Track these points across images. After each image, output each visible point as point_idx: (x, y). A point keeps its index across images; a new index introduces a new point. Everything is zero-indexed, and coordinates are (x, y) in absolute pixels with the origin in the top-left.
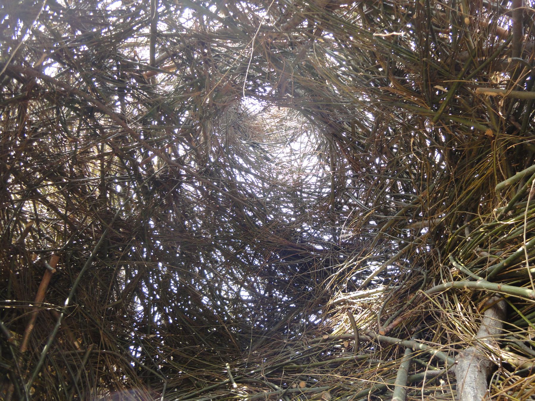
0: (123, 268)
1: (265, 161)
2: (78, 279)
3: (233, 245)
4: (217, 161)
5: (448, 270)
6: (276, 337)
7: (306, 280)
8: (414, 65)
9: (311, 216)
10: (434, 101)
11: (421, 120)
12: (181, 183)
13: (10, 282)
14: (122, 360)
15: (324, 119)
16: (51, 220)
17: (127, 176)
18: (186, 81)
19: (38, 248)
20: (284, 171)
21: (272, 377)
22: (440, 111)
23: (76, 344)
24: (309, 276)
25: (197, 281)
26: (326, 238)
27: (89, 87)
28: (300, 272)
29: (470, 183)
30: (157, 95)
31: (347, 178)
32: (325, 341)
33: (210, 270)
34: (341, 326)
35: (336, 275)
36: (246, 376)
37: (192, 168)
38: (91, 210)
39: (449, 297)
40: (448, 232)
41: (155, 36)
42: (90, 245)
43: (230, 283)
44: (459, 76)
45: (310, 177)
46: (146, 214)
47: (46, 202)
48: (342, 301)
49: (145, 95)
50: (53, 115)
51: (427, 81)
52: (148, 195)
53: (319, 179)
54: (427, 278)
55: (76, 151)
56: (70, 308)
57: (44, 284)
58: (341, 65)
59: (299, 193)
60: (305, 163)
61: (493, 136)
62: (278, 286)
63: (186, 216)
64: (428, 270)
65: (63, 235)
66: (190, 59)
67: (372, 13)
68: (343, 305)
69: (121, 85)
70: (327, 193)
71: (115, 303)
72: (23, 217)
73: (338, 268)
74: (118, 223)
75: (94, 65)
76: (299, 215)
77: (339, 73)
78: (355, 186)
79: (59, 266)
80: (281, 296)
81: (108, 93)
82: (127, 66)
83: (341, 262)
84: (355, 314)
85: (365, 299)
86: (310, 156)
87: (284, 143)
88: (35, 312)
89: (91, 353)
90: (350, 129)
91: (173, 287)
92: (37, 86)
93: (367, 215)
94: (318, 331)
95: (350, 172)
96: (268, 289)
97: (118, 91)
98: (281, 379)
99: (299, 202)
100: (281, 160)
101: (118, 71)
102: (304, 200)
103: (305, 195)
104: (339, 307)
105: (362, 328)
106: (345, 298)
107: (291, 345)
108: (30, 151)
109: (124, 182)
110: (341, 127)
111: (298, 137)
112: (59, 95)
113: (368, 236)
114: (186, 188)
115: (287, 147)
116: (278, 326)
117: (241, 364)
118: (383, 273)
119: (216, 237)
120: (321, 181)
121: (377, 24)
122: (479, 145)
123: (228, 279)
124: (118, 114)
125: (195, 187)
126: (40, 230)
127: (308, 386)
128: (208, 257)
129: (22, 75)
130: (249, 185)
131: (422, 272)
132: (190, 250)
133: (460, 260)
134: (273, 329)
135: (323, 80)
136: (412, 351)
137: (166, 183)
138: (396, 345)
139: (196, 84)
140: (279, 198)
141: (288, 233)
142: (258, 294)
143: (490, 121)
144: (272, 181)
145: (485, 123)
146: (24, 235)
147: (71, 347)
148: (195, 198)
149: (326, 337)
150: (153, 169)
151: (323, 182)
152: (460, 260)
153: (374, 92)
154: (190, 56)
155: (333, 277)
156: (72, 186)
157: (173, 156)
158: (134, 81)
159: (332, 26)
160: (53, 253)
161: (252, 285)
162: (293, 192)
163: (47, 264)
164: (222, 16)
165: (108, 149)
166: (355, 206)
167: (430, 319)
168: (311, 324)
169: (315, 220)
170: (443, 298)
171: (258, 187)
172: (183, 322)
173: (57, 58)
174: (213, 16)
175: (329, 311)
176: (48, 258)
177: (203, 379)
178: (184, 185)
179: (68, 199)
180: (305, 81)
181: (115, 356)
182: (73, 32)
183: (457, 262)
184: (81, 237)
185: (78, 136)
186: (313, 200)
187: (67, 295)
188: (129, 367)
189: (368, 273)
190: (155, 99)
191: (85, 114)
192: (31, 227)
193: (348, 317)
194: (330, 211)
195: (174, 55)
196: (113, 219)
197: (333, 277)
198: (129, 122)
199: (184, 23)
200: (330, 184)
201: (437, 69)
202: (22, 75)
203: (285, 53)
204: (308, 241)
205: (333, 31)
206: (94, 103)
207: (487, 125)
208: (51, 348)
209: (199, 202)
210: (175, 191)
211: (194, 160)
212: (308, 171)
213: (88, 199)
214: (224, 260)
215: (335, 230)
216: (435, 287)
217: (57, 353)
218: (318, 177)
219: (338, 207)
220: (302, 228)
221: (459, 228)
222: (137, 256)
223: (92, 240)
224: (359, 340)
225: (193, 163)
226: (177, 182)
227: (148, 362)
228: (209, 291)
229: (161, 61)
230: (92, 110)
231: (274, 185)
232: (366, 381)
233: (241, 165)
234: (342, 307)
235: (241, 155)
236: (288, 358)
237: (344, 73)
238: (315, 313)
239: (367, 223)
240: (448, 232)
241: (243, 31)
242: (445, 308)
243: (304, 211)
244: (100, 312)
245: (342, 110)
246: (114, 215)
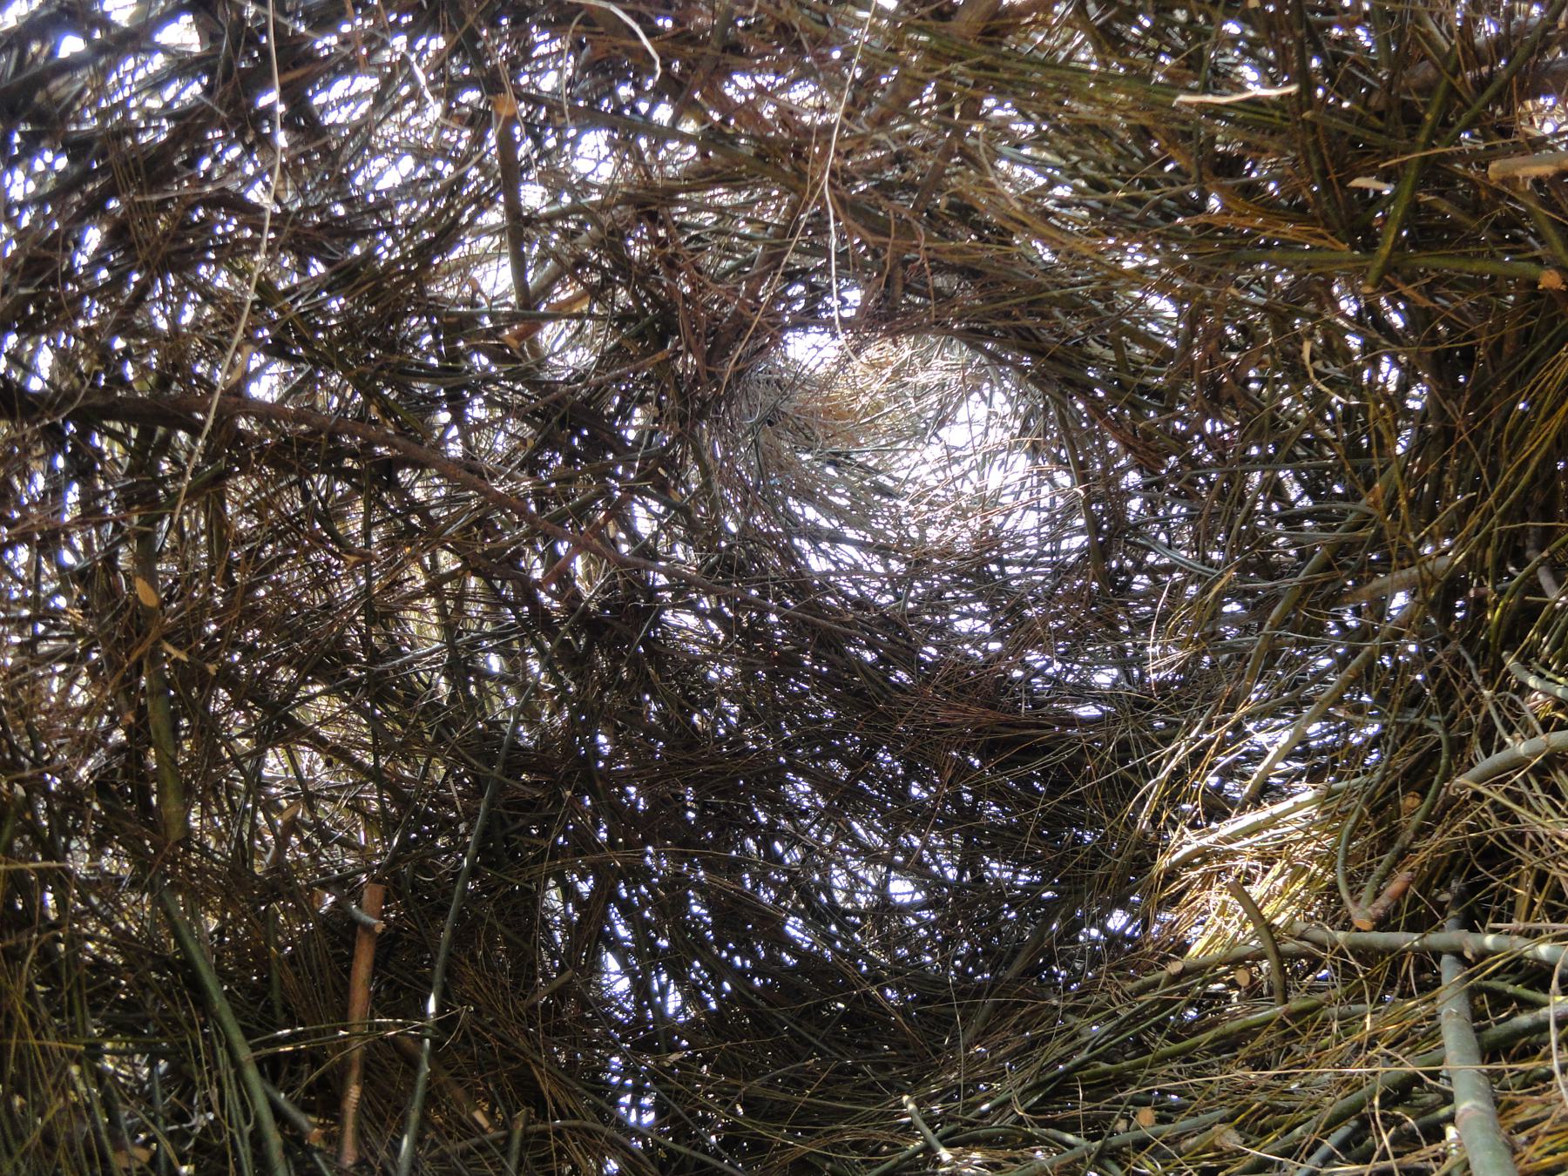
2: (445, 936)
4: (745, 527)
5: (1512, 702)
6: (1022, 994)
7: (1072, 810)
8: (1272, 134)
9: (1044, 625)
10: (1356, 222)
11: (1320, 284)
12: (661, 611)
13: (275, 977)
14: (610, 1140)
15: (1027, 341)
16: (340, 788)
19: (325, 873)
20: (941, 515)
21: (1044, 1112)
22: (1384, 251)
23: (479, 1116)
24: (1078, 800)
25: (761, 878)
26: (1104, 678)
27: (373, 408)
28: (1051, 794)
30: (550, 386)
32: (1175, 979)
33: (792, 840)
34: (1210, 927)
38: (439, 739)
39: (1540, 781)
41: (520, 226)
42: (453, 835)
43: (853, 864)
44: (1422, 138)
45: (1016, 516)
46: (588, 716)
47: (319, 743)
48: (1195, 853)
50: (292, 502)
52: (577, 663)
53: (1044, 515)
54: (1450, 740)
55: (369, 585)
56: (445, 1024)
58: (1052, 183)
59: (994, 568)
60: (994, 478)
62: (993, 846)
63: (693, 701)
65: (382, 824)
66: (623, 264)
67: (1117, 18)
69: (452, 381)
71: (556, 984)
72: (268, 795)
73: (1159, 762)
74: (517, 758)
75: (372, 342)
76: (1010, 631)
77: (1049, 204)
78: (1155, 513)
80: (1007, 875)
81: (422, 410)
82: (456, 325)
83: (1167, 741)
87: (918, 435)
88: (357, 1049)
89: (526, 1135)
90: (1110, 355)
92: (241, 435)
93: (1216, 589)
94: (1145, 955)
95: (1133, 478)
96: (969, 862)
98: (1079, 1112)
99: (1000, 592)
101: (436, 344)
102: (1014, 583)
104: (1192, 874)
106: (1204, 842)
107: (1073, 1010)
108: (252, 615)
109: (509, 644)
111: (957, 407)
112: (299, 447)
113: (1228, 648)
114: (674, 621)
116: (1019, 965)
118: (1300, 750)
120: (1050, 521)
121: (1137, 45)
122: (1521, 322)
123: (844, 853)
124: (456, 461)
125: (701, 614)
127: (1161, 1120)
128: (779, 804)
131: (1427, 723)
132: (723, 791)
133: (1548, 667)
134: (1009, 975)
135: (1003, 236)
136: (1467, 963)
139: (648, 331)
140: (940, 593)
141: (982, 687)
142: (941, 881)
143: (1542, 243)
144: (912, 549)
146: (282, 843)
147: (471, 1129)
149: (1175, 967)
151: (1058, 524)
152: (1548, 667)
153: (1167, 238)
154: (622, 258)
158: (485, 361)
159: (1009, 82)
160: (364, 878)
161: (920, 861)
162: (978, 571)
165: (448, 561)
166: (1169, 569)
167: (1495, 856)
168: (1114, 940)
169: (1060, 634)
170: (1523, 789)
171: (873, 575)
172: (750, 1004)
173: (276, 350)
174: (662, 135)
176: (356, 893)
177: (846, 1151)
178: (668, 616)
180: (960, 251)
181: (590, 1133)
182: (303, 268)
183: (1541, 676)
185: (369, 543)
187: (430, 986)
188: (632, 1153)
189: (1256, 756)
191: (375, 479)
192: (294, 818)
194: (1098, 597)
198: (493, 476)
200: (1080, 522)
203: (886, 188)
205: (1015, 94)
207: (1538, 260)
208: (419, 1141)
209: (718, 653)
212: (1007, 500)
213: (424, 712)
215: (1123, 650)
216: (1484, 764)
217: (435, 1152)
218: (1039, 510)
220: (1025, 666)
221: (1520, 575)
225: (679, 548)
226: (648, 610)
227: (682, 1133)
228: (801, 898)
229: (545, 290)
230: (389, 467)
231: (919, 565)
233: (814, 523)
235: (807, 496)
236: (1079, 1049)
237: (1063, 203)
238: (1122, 903)
239: (1216, 615)
241: (757, 155)
243: (1021, 617)
245: (1073, 306)
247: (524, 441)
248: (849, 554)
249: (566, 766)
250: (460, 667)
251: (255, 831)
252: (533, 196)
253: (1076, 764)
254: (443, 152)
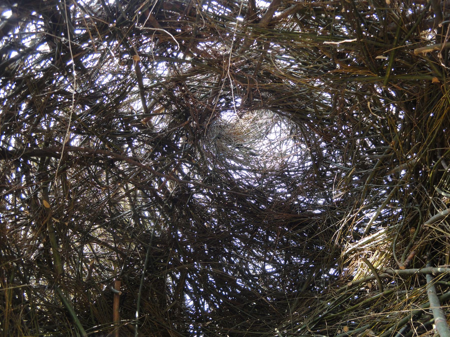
1: (251, 156)
4: (214, 169)
9: (302, 188)
10: (379, 68)
13: (91, 311)
15: (289, 109)
16: (106, 254)
17: (150, 203)
19: (103, 279)
24: (317, 237)
25: (228, 268)
28: (309, 237)
31: (322, 149)
32: (350, 287)
33: (236, 257)
34: (359, 271)
37: (198, 180)
38: (133, 237)
40: (426, 168)
41: (143, 90)
42: (139, 264)
44: (395, 44)
45: (291, 158)
46: (174, 227)
47: (98, 242)
48: (352, 250)
49: (147, 137)
50: (86, 174)
51: (368, 55)
52: (170, 211)
53: (299, 157)
54: (422, 212)
56: (141, 320)
57: (116, 305)
59: (286, 173)
61: (439, 82)
62: (294, 253)
63: (204, 219)
64: (419, 203)
65: (118, 263)
67: (305, 18)
69: (128, 136)
70: (310, 166)
71: (172, 305)
73: (339, 224)
74: (155, 241)
76: (293, 191)
77: (291, 70)
79: (122, 288)
82: (128, 120)
84: (368, 257)
85: (372, 243)
86: (286, 141)
87: (261, 137)
90: (313, 110)
91: (210, 279)
94: (341, 281)
95: (323, 144)
97: (127, 140)
99: (289, 180)
100: (264, 151)
102: (293, 177)
103: (292, 173)
104: (352, 256)
105: (378, 268)
106: (354, 247)
107: (322, 299)
112: (86, 158)
114: (197, 197)
115: (265, 139)
116: (305, 287)
117: (286, 326)
118: (379, 217)
120: (301, 158)
123: (251, 259)
124: (131, 158)
125: (204, 194)
126: (100, 265)
127: (350, 329)
130: (245, 179)
133: (447, 189)
136: (434, 277)
137: (181, 198)
138: (415, 274)
141: (286, 208)
143: (431, 70)
145: (429, 73)
146: (90, 271)
148: (206, 203)
149: (350, 284)
150: (168, 191)
151: (303, 159)
152: (447, 189)
155: (338, 232)
156: (114, 223)
157: (180, 176)
158: (137, 129)
159: (277, 38)
160: (114, 279)
162: (282, 174)
163: (113, 289)
164: (188, 58)
166: (336, 169)
170: (444, 225)
171: (252, 178)
173: (78, 132)
175: (344, 261)
176: (113, 284)
178: (195, 196)
179: (114, 234)
182: (83, 108)
184: (131, 260)
186: (300, 175)
187: (136, 309)
189: (367, 220)
190: (156, 137)
191: (108, 165)
192: (93, 264)
193: (362, 262)
194: (316, 179)
195: (160, 100)
196: (151, 239)
197: (338, 232)
198: (142, 161)
199: (162, 74)
200: (310, 158)
201: (372, 44)
203: (245, 70)
204: (307, 210)
207: (431, 75)
209: (210, 205)
211: (197, 174)
213: (128, 230)
215: (326, 193)
216: (432, 218)
218: (297, 155)
219: (321, 175)
220: (298, 200)
222: (176, 263)
224: (380, 278)
225: (196, 176)
226: (189, 195)
228: (240, 273)
229: (152, 107)
230: (112, 161)
231: (265, 174)
232: (402, 311)
233: (234, 165)
234: (354, 255)
235: (231, 158)
236: (325, 310)
237: (295, 70)
238: (333, 266)
239: (351, 180)
240: (426, 168)
243: (296, 186)
244: (162, 315)
245: (301, 98)
246: (150, 236)
247: (149, 150)
248: (245, 173)
249: (170, 241)
250: (137, 216)
251: (82, 269)
252: (146, 82)
254: (120, 72)
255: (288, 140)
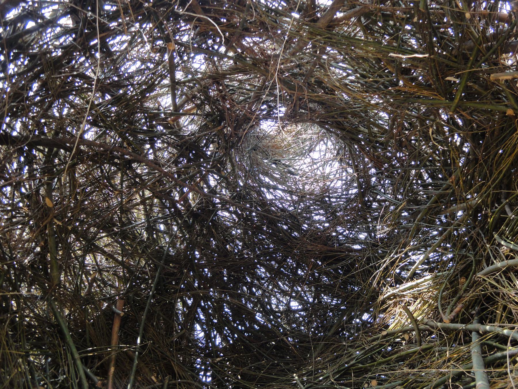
0: (179, 300)
3: (275, 259)
4: (245, 184)
9: (343, 218)
10: (447, 91)
15: (339, 126)
16: (110, 268)
18: (207, 118)
19: (105, 296)
22: (456, 101)
23: (153, 378)
24: (353, 276)
26: (362, 236)
28: (344, 274)
29: (500, 163)
30: (183, 137)
31: (371, 176)
32: (384, 337)
34: (396, 320)
35: (380, 271)
36: (316, 384)
38: (143, 252)
39: (505, 276)
41: (175, 85)
44: (469, 65)
46: (192, 246)
47: (104, 253)
48: (391, 295)
50: (98, 173)
51: (437, 75)
53: (344, 182)
54: (476, 260)
56: (143, 347)
59: (327, 199)
65: (123, 280)
67: (371, 23)
68: (393, 299)
69: (151, 135)
70: (355, 194)
71: (180, 334)
74: (169, 259)
76: (332, 220)
77: (347, 82)
81: (141, 144)
82: (153, 116)
87: (303, 154)
88: (113, 355)
89: (169, 385)
90: (366, 131)
91: (226, 310)
94: (374, 329)
95: (373, 171)
97: (149, 140)
99: (329, 207)
100: (304, 171)
106: (394, 291)
107: (350, 346)
108: (83, 210)
110: (357, 130)
112: (100, 155)
114: (222, 215)
116: (332, 331)
119: (258, 256)
120: (346, 184)
123: (276, 292)
124: (151, 161)
125: (230, 212)
128: (254, 276)
129: (68, 145)
130: (279, 200)
133: (508, 238)
139: (215, 119)
140: (309, 207)
141: (322, 238)
142: (307, 302)
146: (91, 285)
148: (232, 222)
149: (384, 333)
151: (348, 185)
152: (508, 238)
158: (162, 128)
159: (336, 43)
160: (117, 298)
161: (301, 295)
162: (322, 200)
164: (231, 54)
165: (148, 193)
166: (384, 201)
167: (490, 299)
169: (348, 221)
170: (499, 278)
171: (287, 200)
172: (243, 342)
173: (94, 124)
174: (222, 57)
176: (115, 303)
179: (122, 246)
182: (103, 97)
183: (505, 241)
184: (139, 278)
189: (412, 263)
191: (125, 166)
192: (95, 277)
194: (360, 210)
196: (164, 257)
198: (163, 166)
200: (355, 185)
202: (68, 145)
203: (294, 75)
206: (131, 156)
207: (506, 106)
209: (236, 225)
210: (213, 219)
213: (138, 243)
214: (268, 275)
215: (369, 227)
216: (487, 269)
218: (342, 180)
219: (367, 206)
220: (336, 231)
221: (499, 207)
223: (148, 279)
224: (419, 330)
225: (224, 190)
226: (213, 211)
228: (261, 307)
229: (182, 106)
230: (130, 162)
231: (302, 197)
233: (268, 183)
235: (266, 174)
236: (352, 359)
238: (368, 311)
241: (253, 64)
242: (504, 287)
243: (336, 215)
245: (355, 115)
246: (163, 252)
247: (174, 155)
248: (279, 193)
249: (185, 262)
250: (151, 228)
251: (82, 281)
252: (179, 75)
253: (353, 265)
254: (150, 60)
255: (333, 161)
